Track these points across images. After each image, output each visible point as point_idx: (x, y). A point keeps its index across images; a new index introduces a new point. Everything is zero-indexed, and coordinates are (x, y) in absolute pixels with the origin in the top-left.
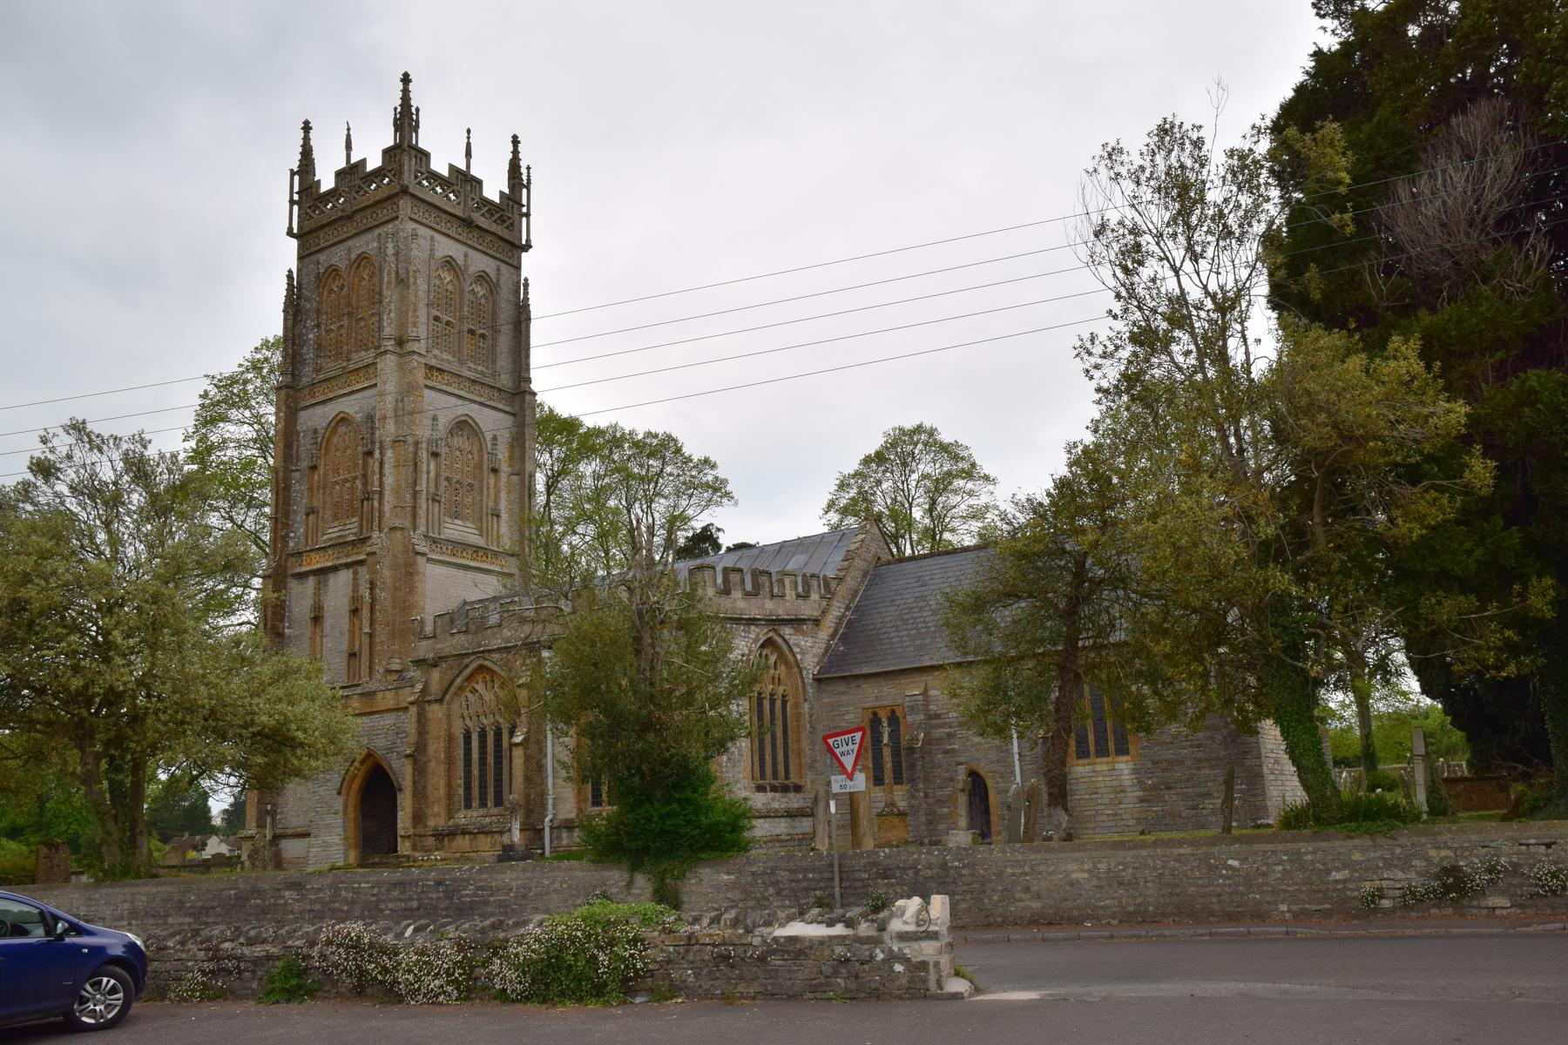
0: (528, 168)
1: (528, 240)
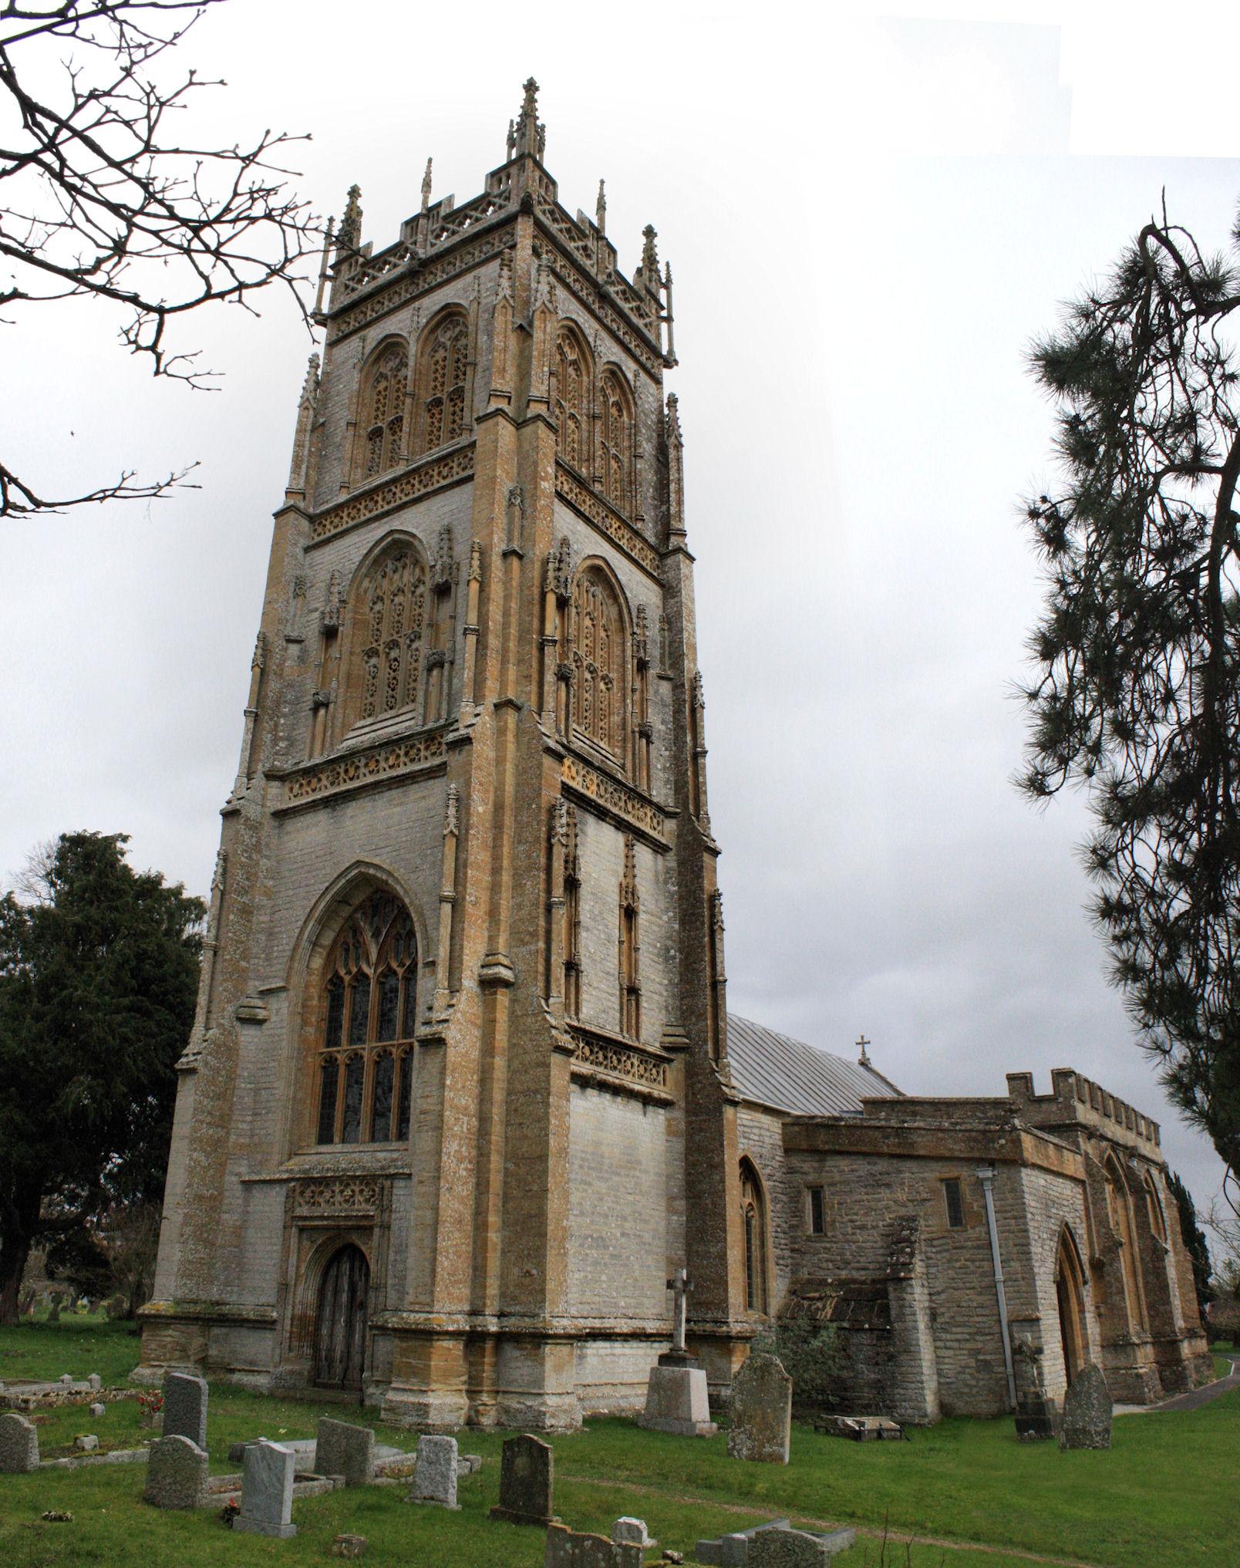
0: (668, 264)
1: (671, 351)
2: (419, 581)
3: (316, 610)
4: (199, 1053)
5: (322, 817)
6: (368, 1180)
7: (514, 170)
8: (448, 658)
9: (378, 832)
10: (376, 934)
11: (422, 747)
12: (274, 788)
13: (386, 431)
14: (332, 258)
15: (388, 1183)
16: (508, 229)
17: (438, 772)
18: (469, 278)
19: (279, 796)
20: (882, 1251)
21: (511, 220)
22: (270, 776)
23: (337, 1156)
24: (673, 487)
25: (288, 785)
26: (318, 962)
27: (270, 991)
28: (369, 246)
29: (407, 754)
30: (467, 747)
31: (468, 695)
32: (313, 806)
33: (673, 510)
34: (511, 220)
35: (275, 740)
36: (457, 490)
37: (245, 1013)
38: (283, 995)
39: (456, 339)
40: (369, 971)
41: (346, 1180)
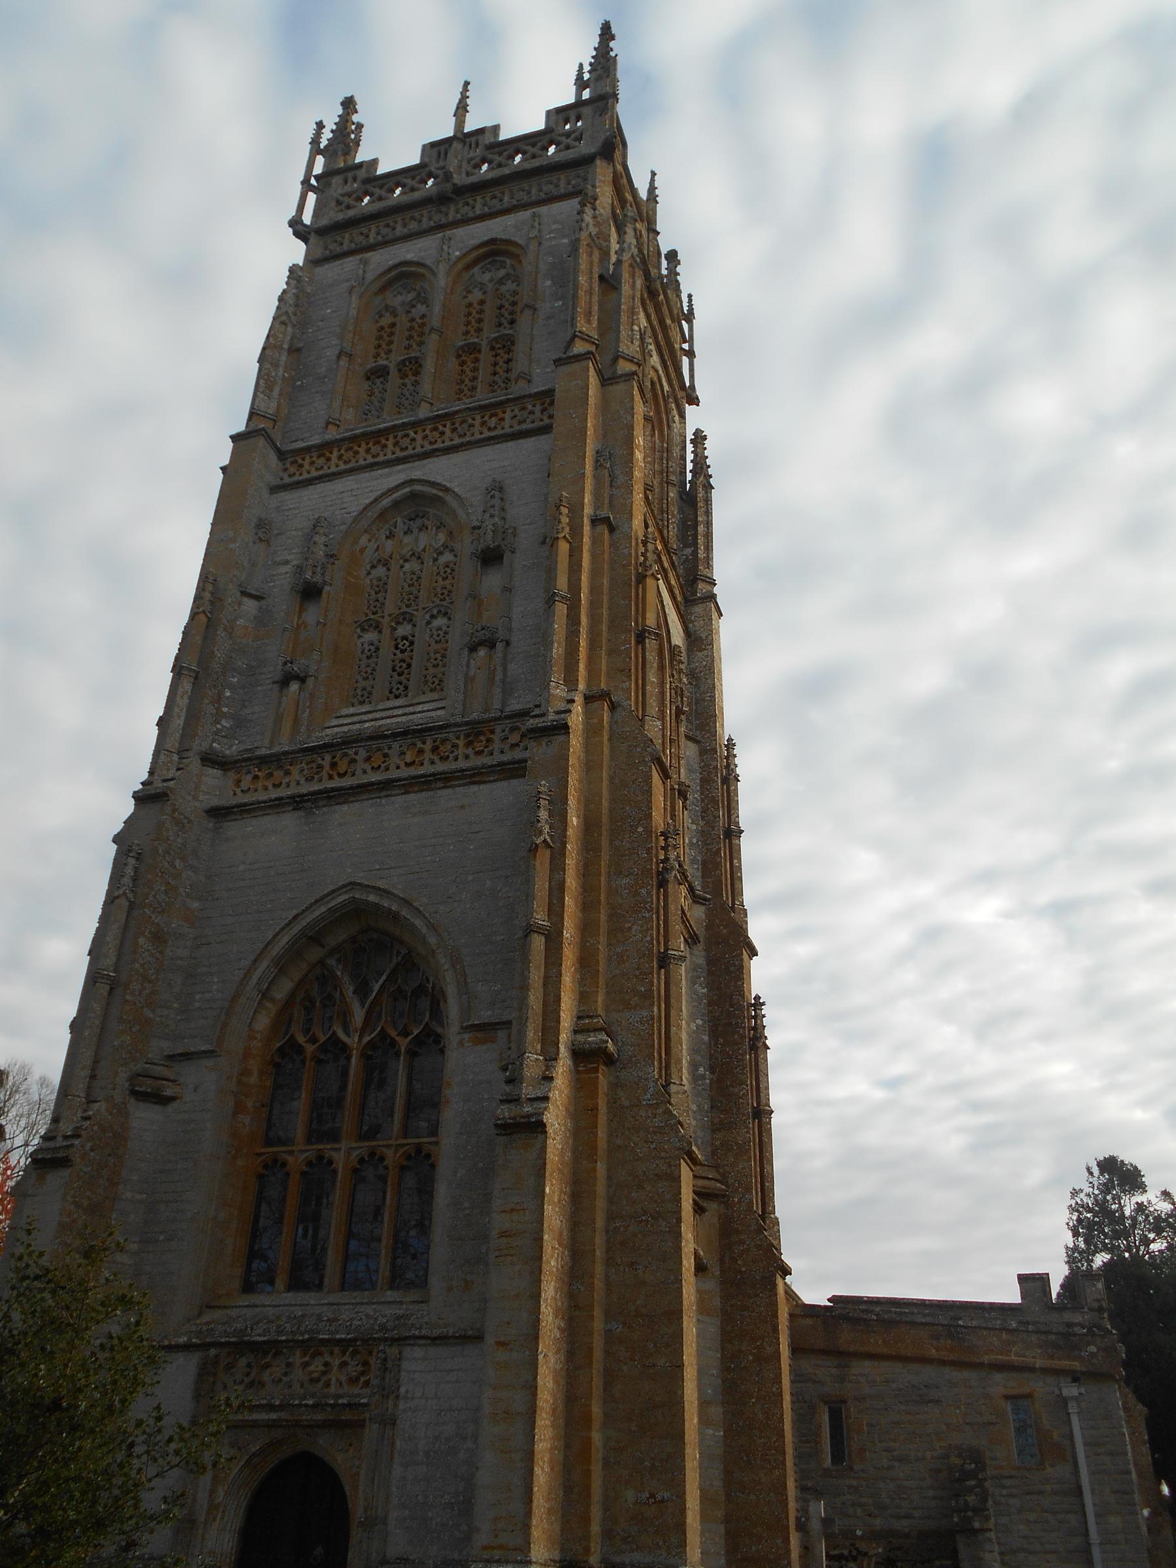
0: (690, 296)
1: (692, 387)
2: (445, 546)
3: (287, 562)
4: (76, 1136)
5: (289, 821)
6: (358, 1346)
7: (587, 111)
8: (501, 634)
9: (383, 845)
10: (362, 990)
11: (461, 743)
12: (213, 777)
13: (393, 371)
14: (318, 169)
15: (393, 1351)
16: (581, 171)
17: (515, 770)
18: (525, 215)
19: (215, 787)
20: (931, 1493)
21: (588, 160)
22: (210, 760)
23: (278, 1308)
24: (701, 528)
25: (232, 775)
26: (263, 1022)
27: (187, 1056)
28: (374, 163)
29: (435, 749)
30: (561, 738)
31: (557, 678)
32: (277, 805)
33: (701, 554)
34: (588, 160)
35: (218, 716)
36: (511, 444)
37: (146, 1086)
38: (210, 1063)
39: (501, 282)
40: (352, 1041)
41: (312, 1346)
